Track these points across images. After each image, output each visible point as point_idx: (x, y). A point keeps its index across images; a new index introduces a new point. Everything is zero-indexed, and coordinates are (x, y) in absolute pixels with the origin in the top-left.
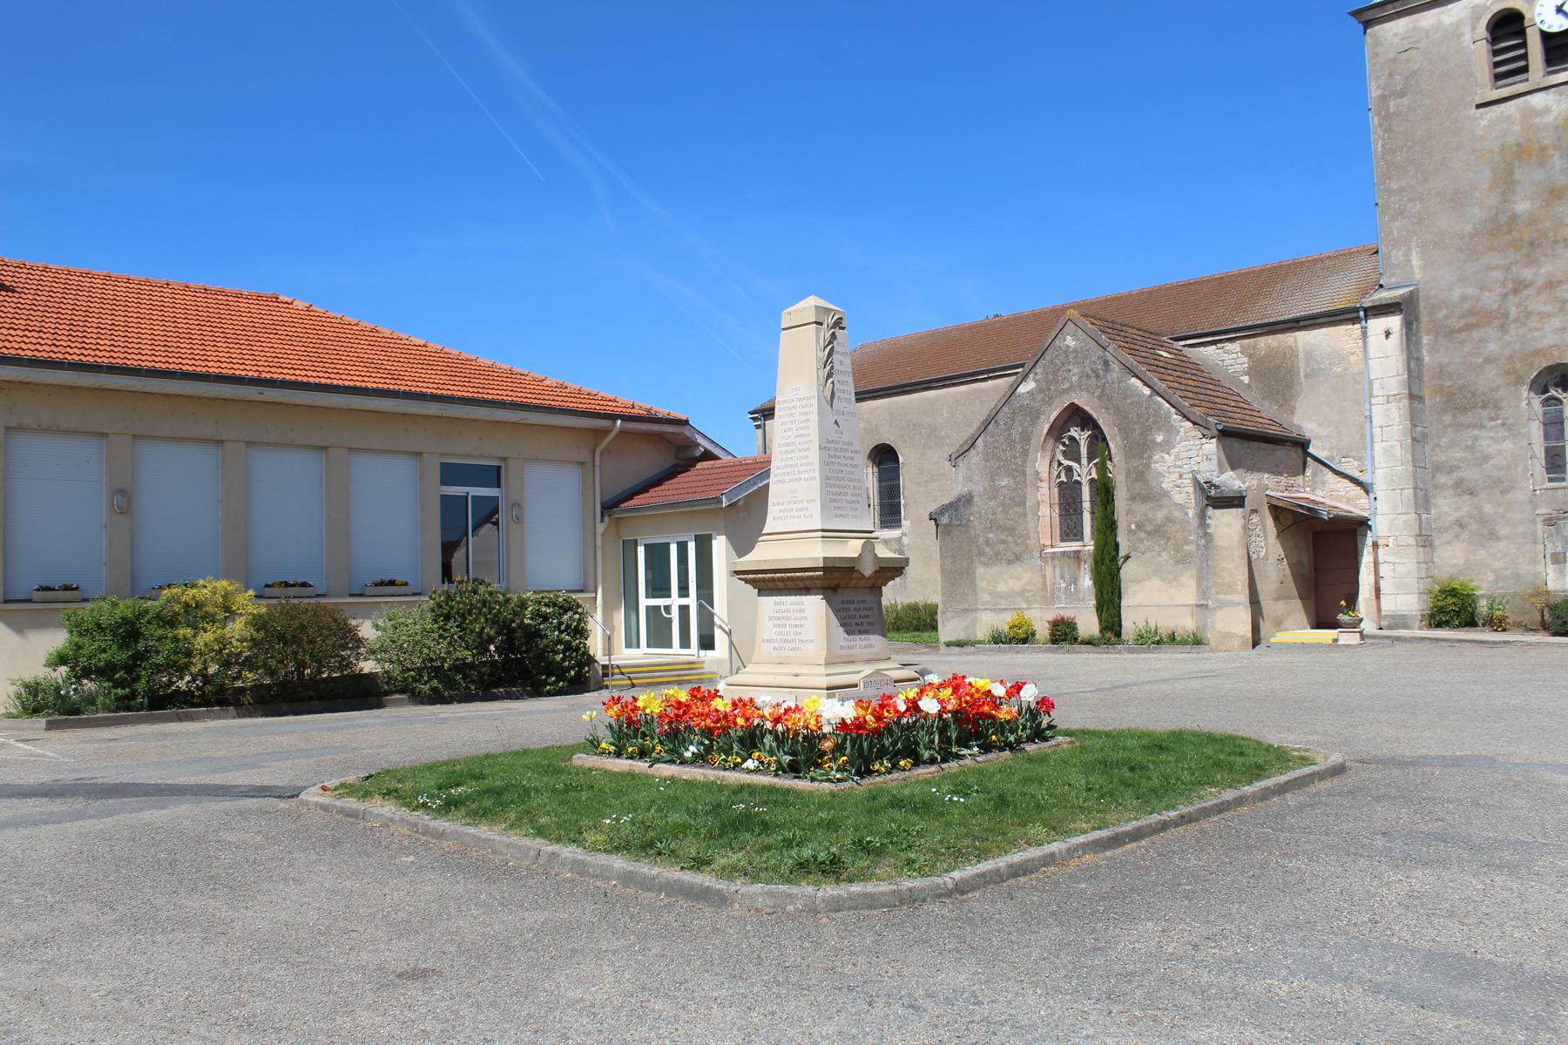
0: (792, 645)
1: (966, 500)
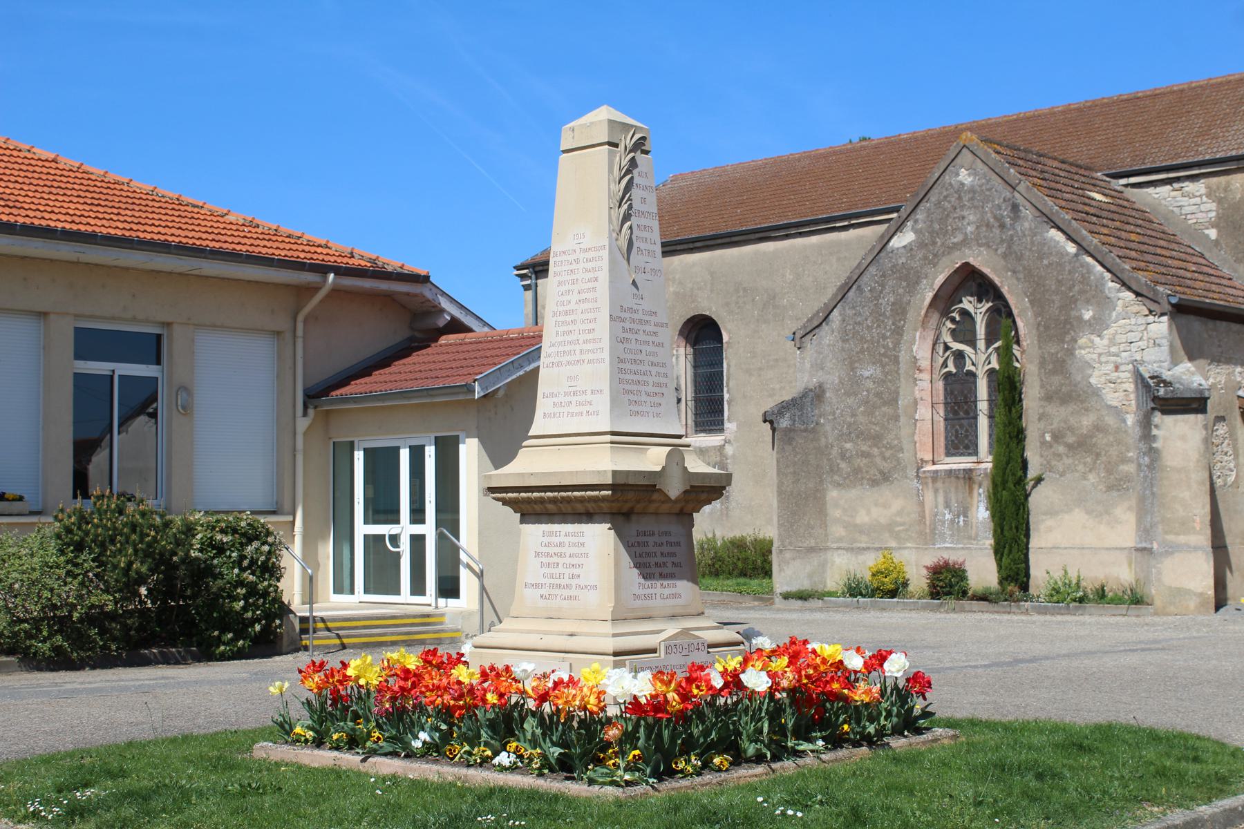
0: (566, 593)
1: (815, 395)
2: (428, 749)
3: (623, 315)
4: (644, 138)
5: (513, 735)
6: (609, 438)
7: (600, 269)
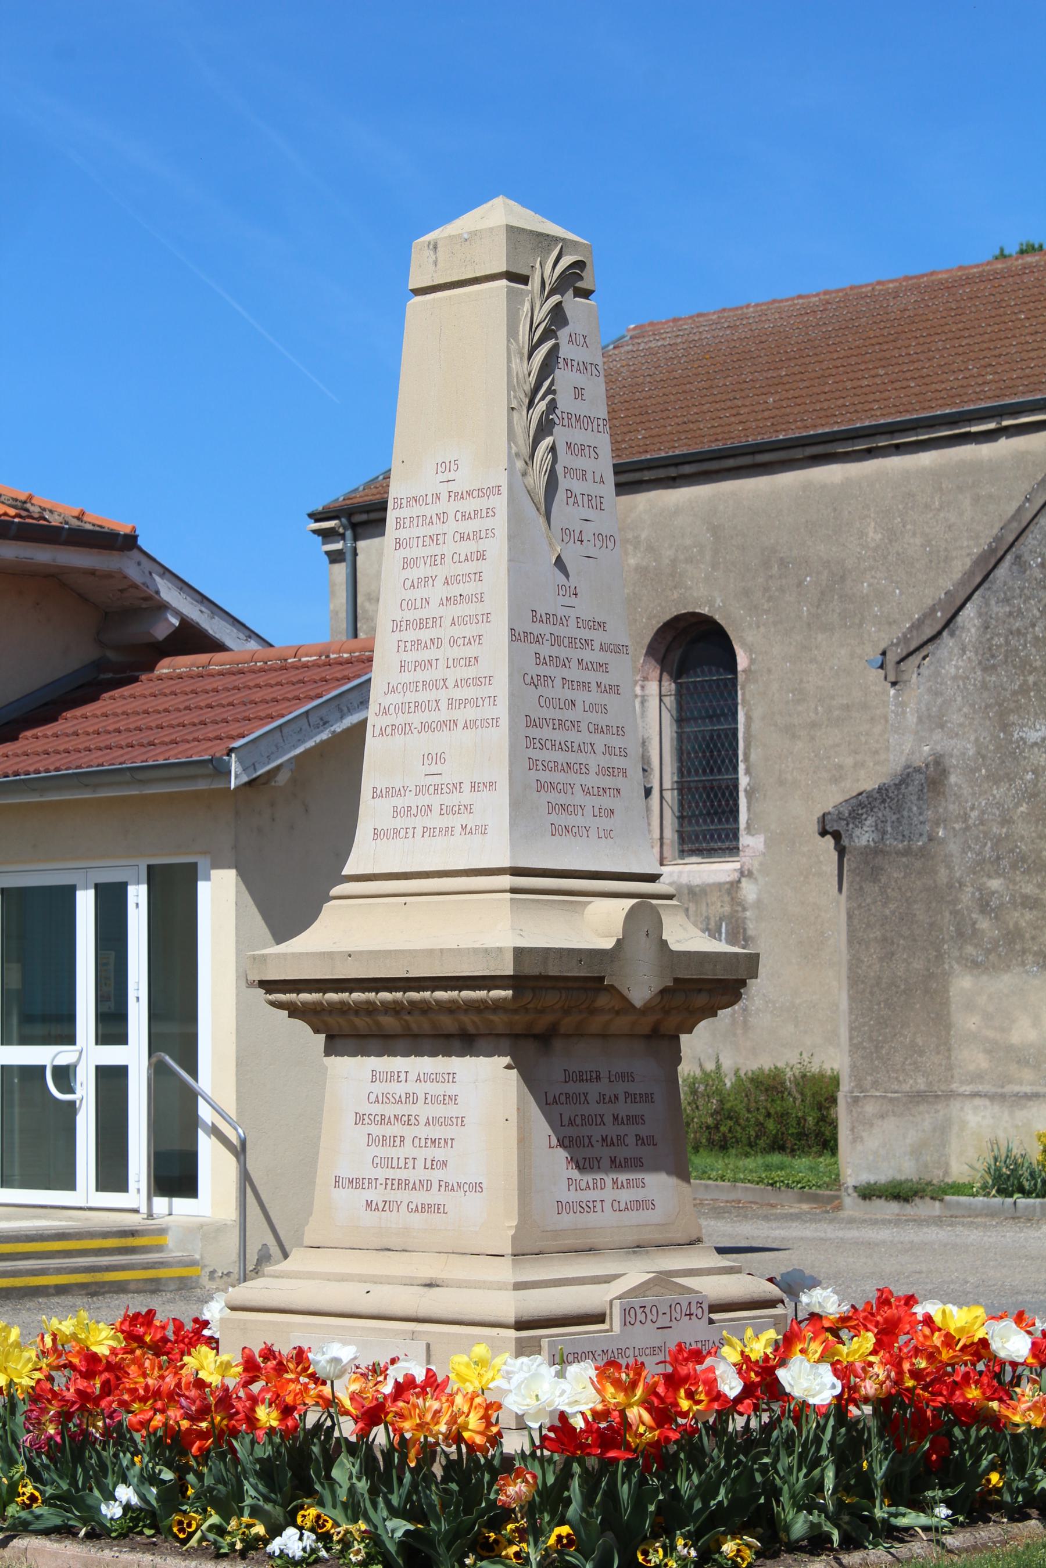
0: (420, 1197)
1: (925, 781)
2: (135, 1520)
3: (538, 628)
4: (580, 265)
5: (311, 1493)
6: (507, 881)
7: (490, 533)
